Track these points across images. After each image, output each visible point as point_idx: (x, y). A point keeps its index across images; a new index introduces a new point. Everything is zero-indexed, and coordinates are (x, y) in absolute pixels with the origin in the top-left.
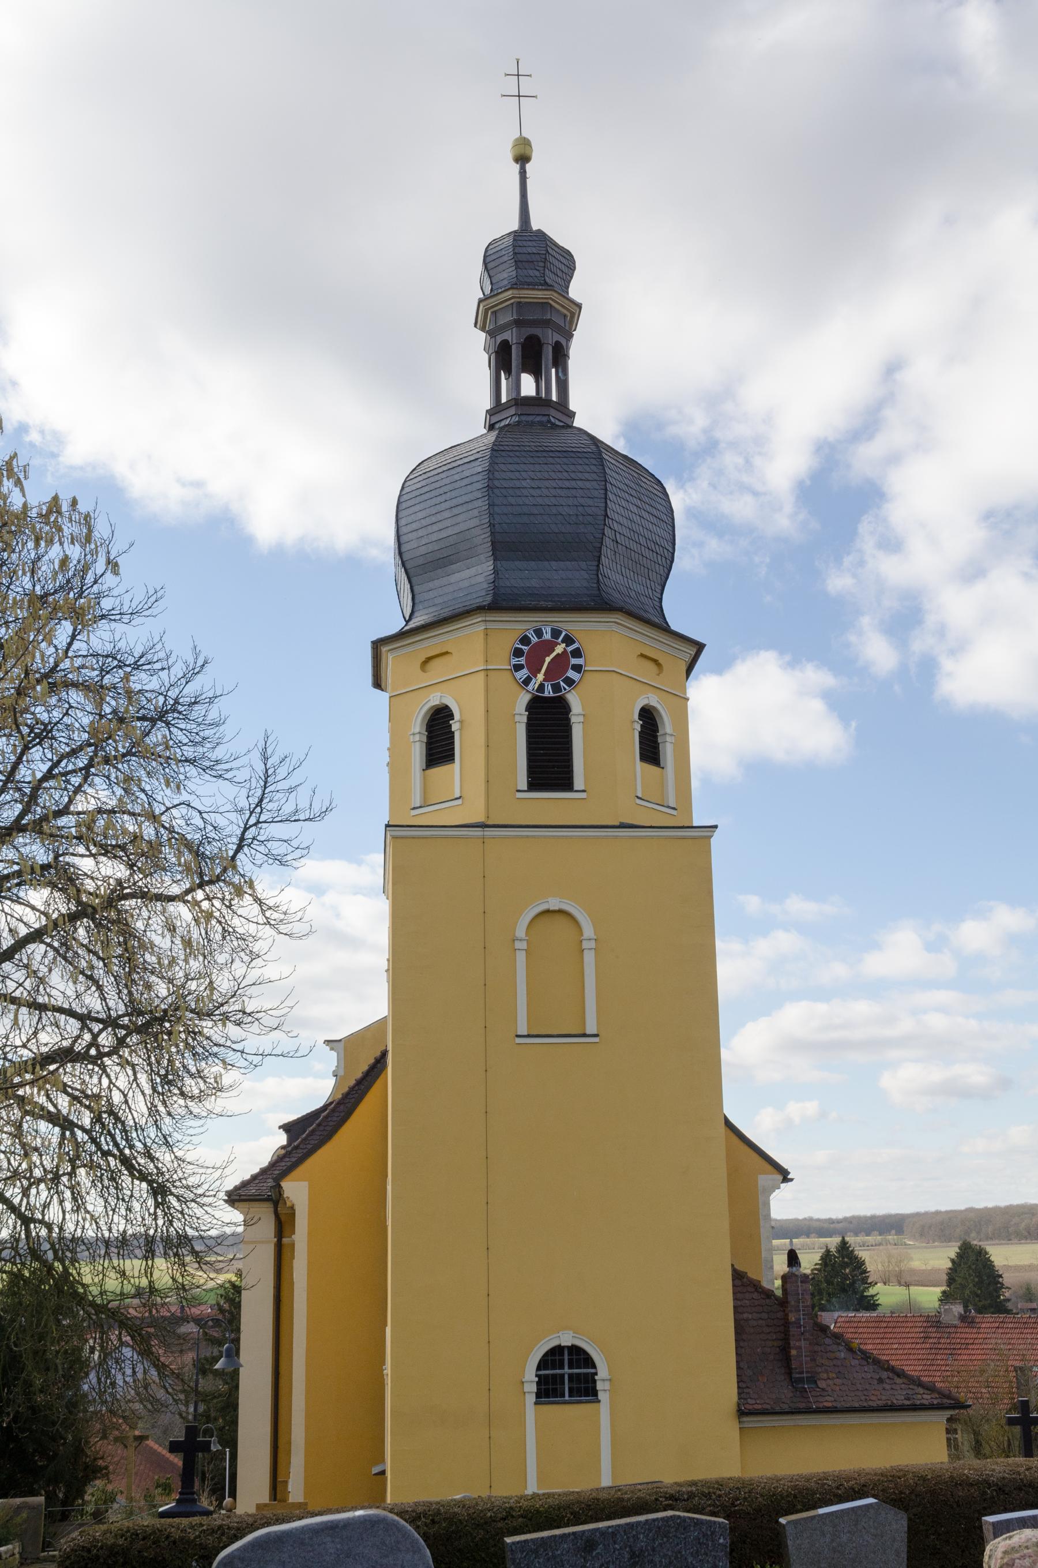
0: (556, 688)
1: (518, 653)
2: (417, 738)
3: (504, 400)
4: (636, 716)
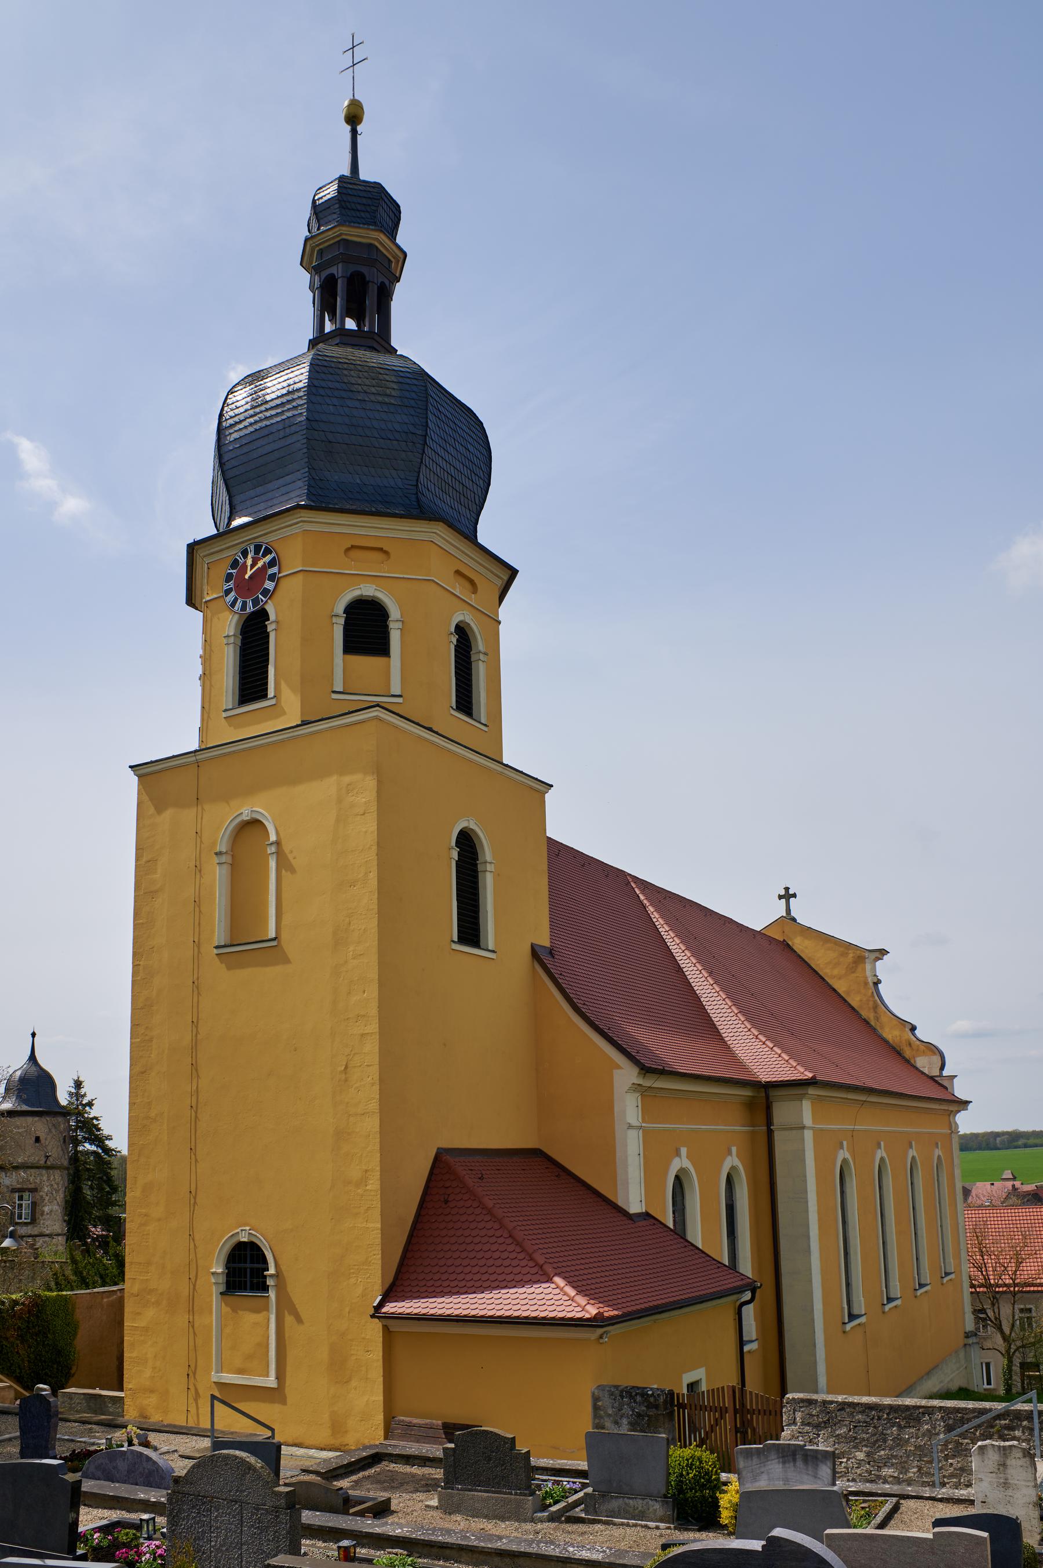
0: (256, 602)
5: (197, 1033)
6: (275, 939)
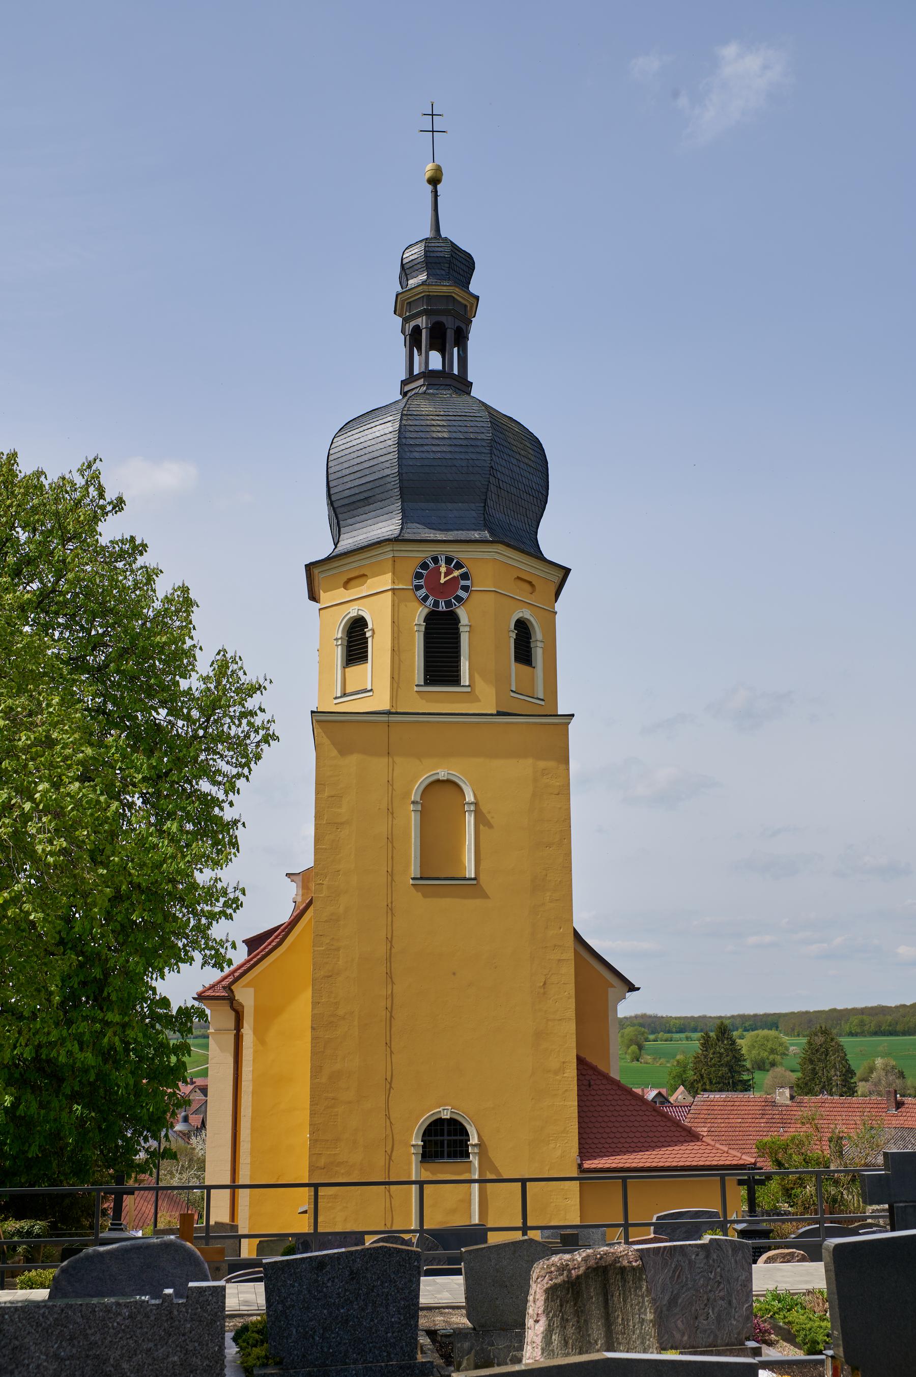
0: (448, 604)
1: (418, 576)
2: (340, 642)
3: (416, 372)
4: (512, 626)
5: (392, 947)
6: (474, 879)
